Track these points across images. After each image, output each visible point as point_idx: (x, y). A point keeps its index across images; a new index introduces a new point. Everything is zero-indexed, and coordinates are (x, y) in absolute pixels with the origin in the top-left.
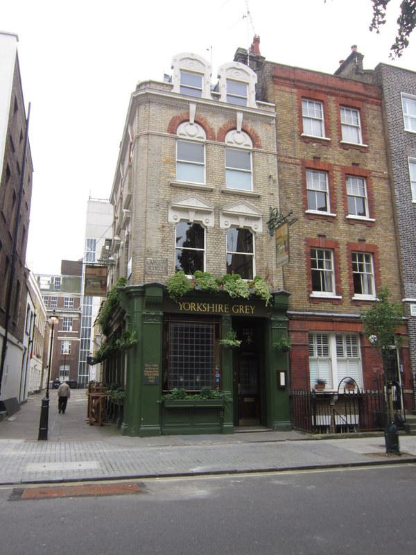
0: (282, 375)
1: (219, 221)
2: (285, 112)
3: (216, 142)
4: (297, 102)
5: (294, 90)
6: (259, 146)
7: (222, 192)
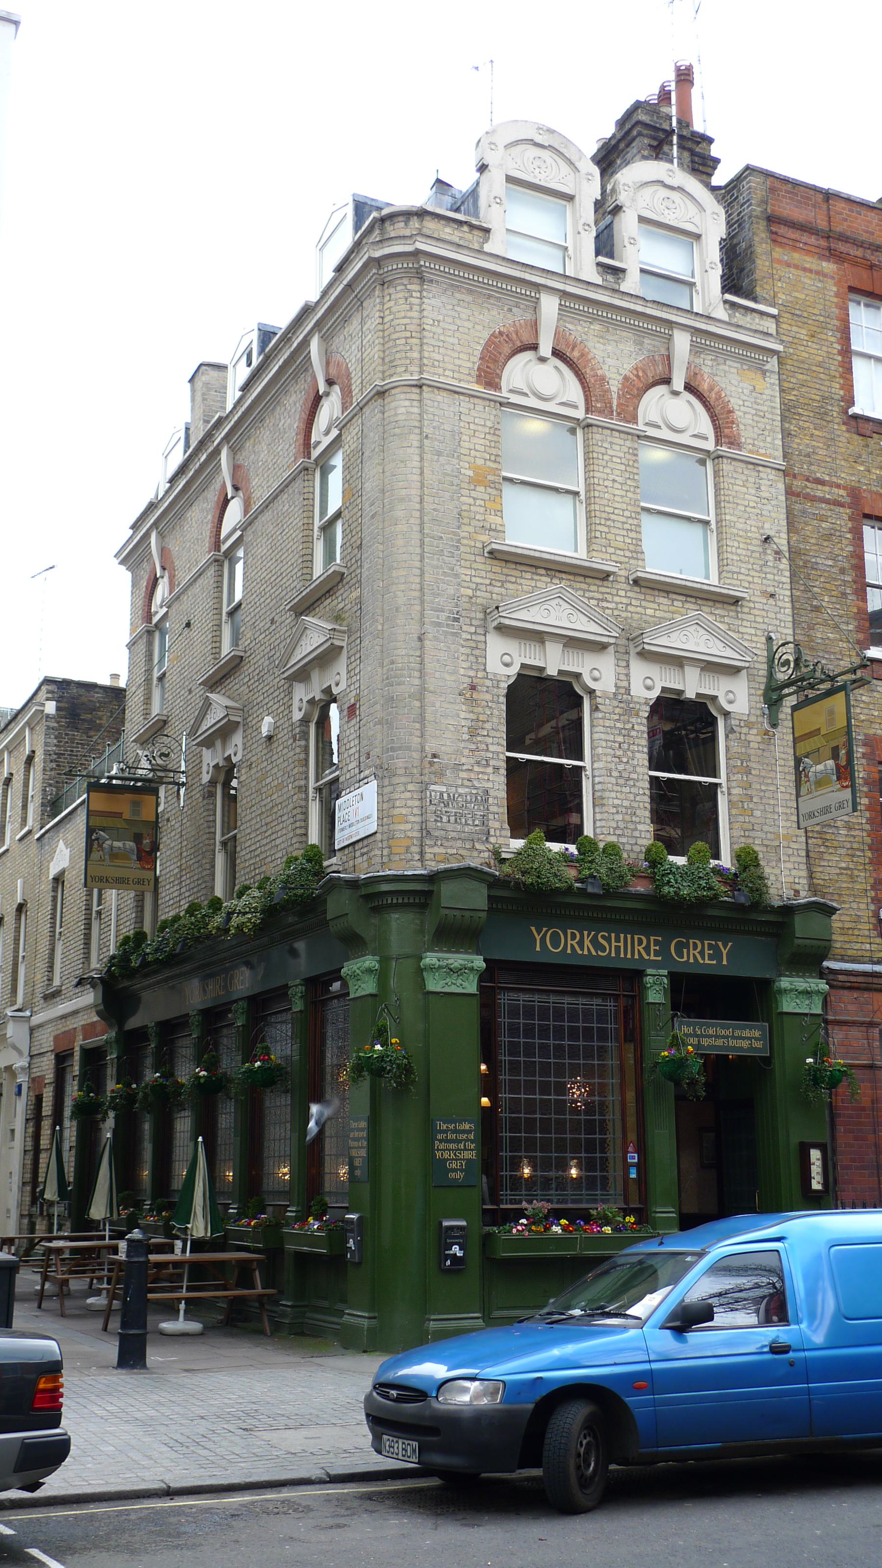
0: (815, 1155)
1: (627, 675)
2: (803, 333)
3: (615, 422)
4: (837, 306)
5: (829, 267)
6: (734, 443)
7: (636, 582)
